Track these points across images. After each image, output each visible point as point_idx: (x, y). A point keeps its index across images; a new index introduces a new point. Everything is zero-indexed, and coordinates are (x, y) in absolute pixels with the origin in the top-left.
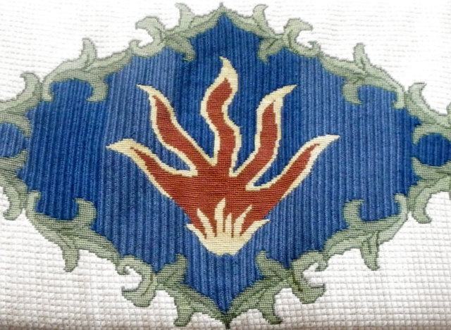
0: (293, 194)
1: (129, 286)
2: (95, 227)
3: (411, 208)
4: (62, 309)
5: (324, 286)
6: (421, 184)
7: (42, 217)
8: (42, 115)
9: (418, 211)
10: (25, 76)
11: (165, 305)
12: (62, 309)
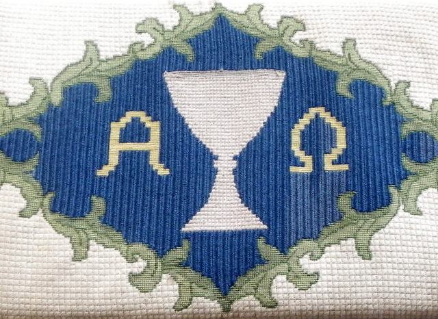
0: (46, 113)
1: (136, 271)
2: (104, 221)
3: (405, 200)
4: (8, 276)
5: (317, 274)
6: (410, 178)
7: (56, 216)
8: (50, 118)
9: (410, 205)
10: (32, 81)
11: (167, 291)
12: (8, 276)
